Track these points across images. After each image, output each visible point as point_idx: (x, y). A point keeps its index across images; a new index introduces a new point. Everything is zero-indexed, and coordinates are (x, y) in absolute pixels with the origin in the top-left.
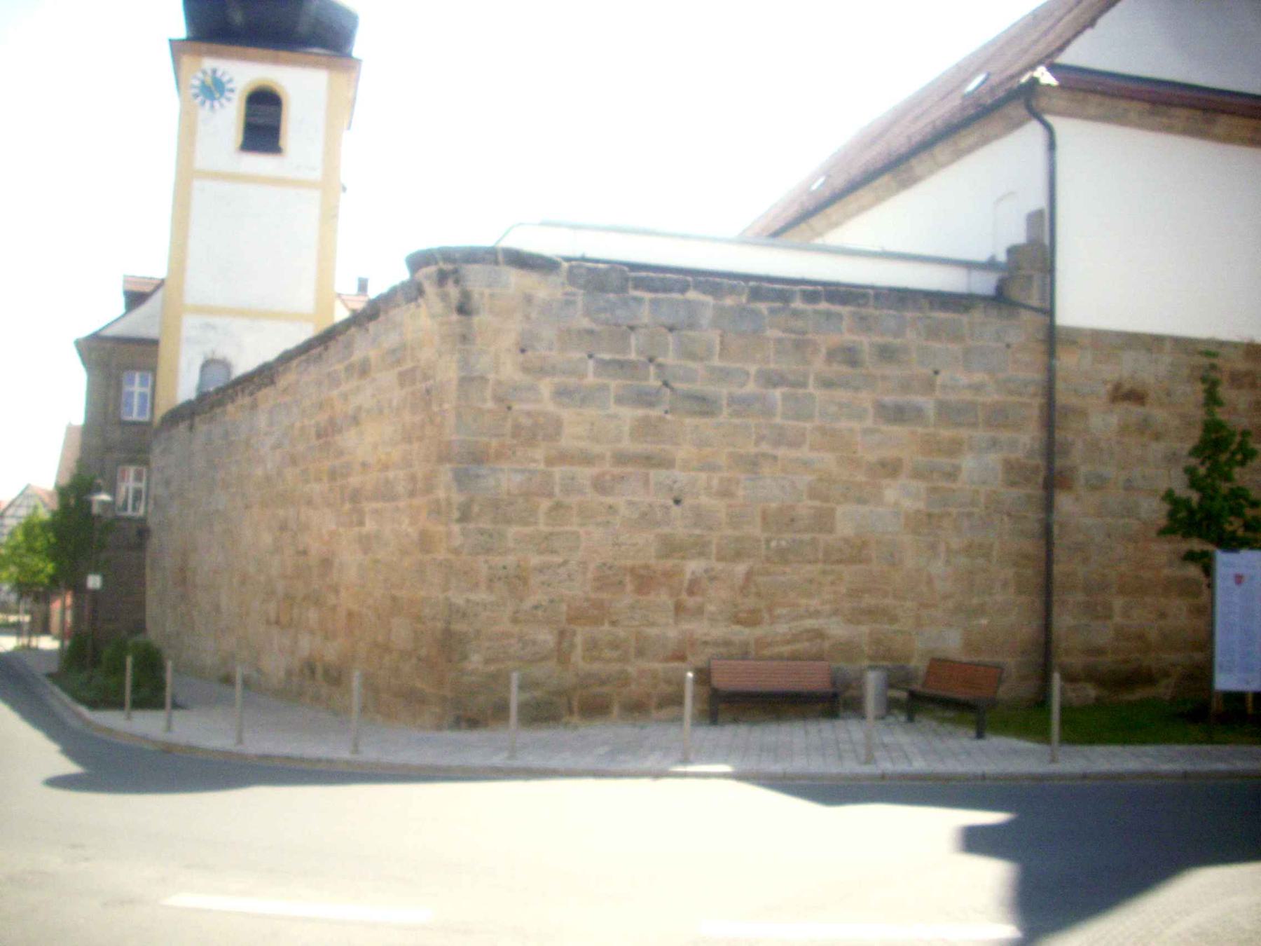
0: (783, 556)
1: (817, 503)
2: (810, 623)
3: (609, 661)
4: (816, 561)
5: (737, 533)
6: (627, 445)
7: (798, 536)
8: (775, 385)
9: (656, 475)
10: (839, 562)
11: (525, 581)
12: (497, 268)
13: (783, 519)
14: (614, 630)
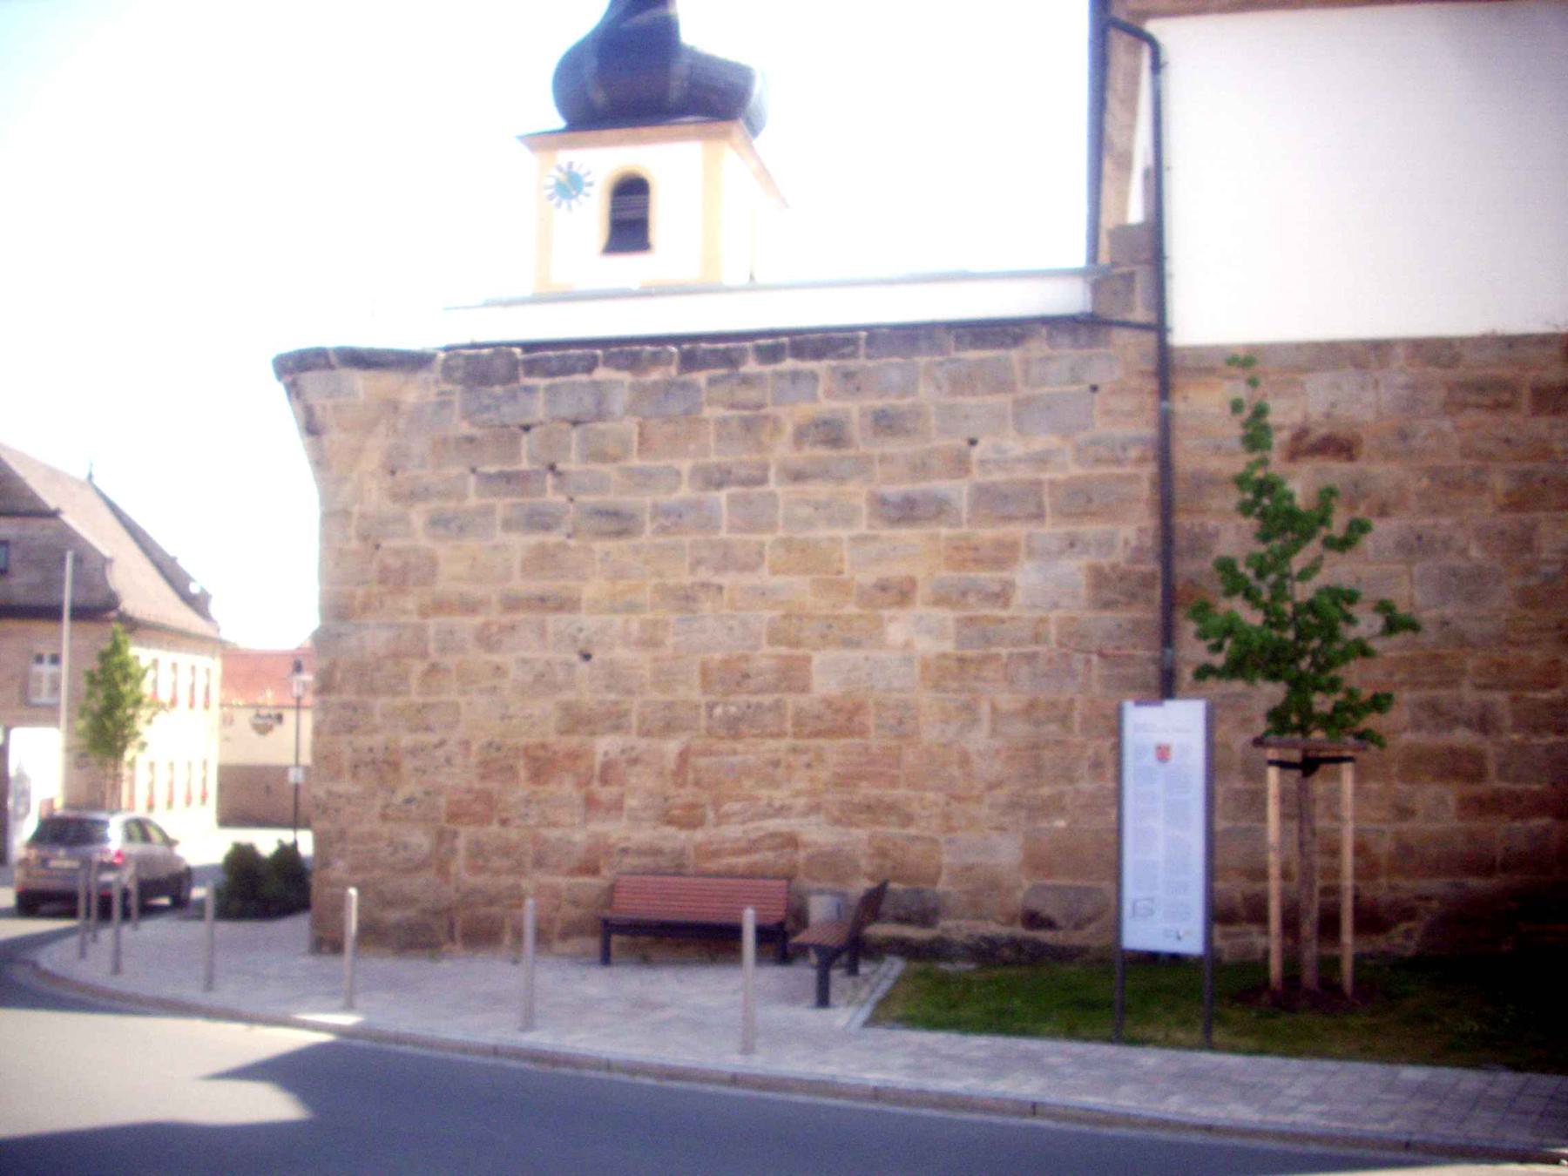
1: (783, 650)
2: (773, 824)
3: (497, 872)
5: (668, 698)
6: (520, 585)
8: (719, 485)
10: (818, 734)
11: (395, 766)
12: (335, 373)
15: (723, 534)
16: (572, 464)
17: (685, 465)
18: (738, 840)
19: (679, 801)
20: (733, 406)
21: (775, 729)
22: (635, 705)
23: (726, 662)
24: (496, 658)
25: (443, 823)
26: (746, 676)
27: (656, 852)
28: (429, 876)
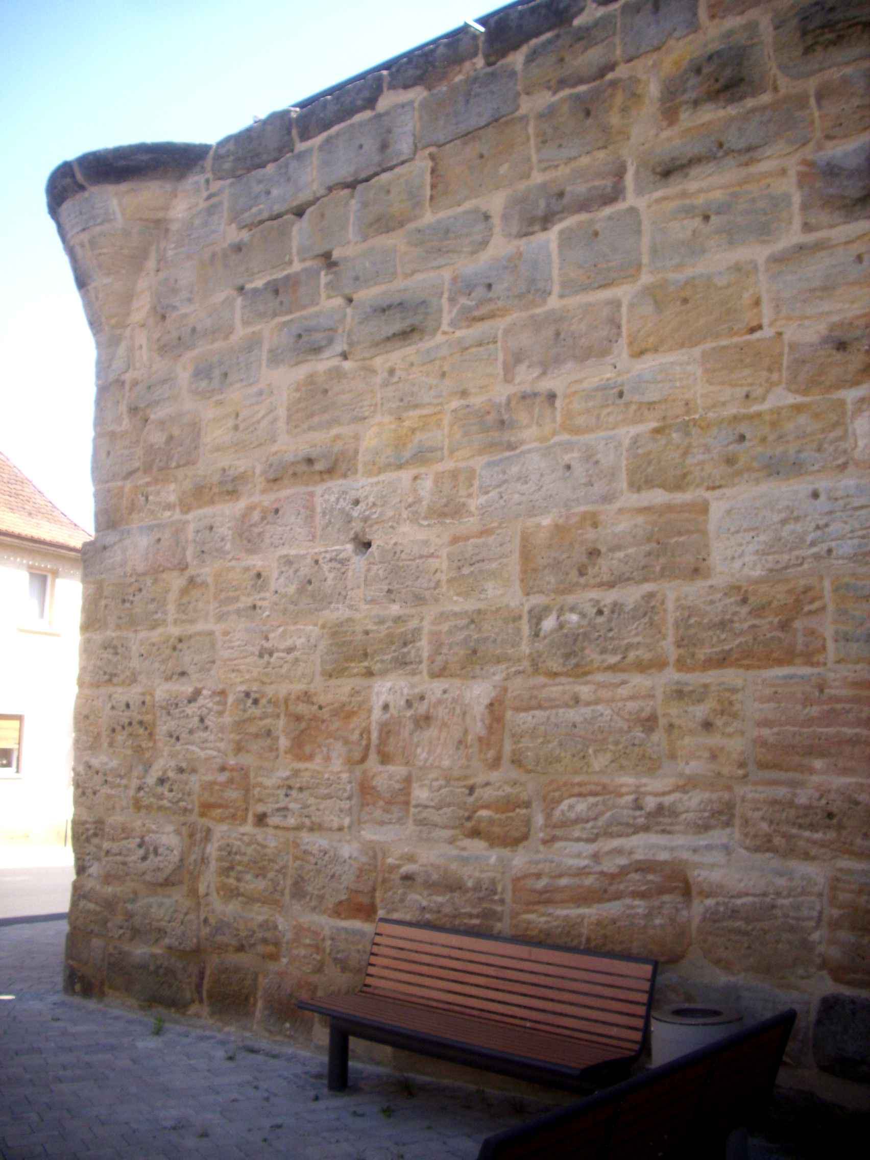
0: (572, 654)
1: (658, 497)
2: (644, 845)
3: (251, 899)
4: (659, 664)
5: (470, 605)
6: (290, 445)
7: (609, 597)
8: (546, 221)
9: (327, 494)
10: (722, 661)
11: (149, 728)
12: (86, 194)
13: (573, 556)
14: (260, 834)
15: (553, 302)
16: (348, 249)
17: (496, 203)
18: (582, 872)
19: (488, 794)
20: (563, 83)
21: (644, 654)
22: (426, 621)
23: (559, 530)
24: (257, 562)
25: (194, 817)
26: (594, 553)
27: (453, 886)
28: (177, 897)
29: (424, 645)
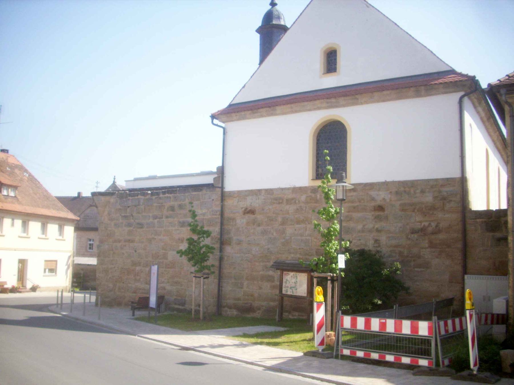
1: (164, 251)
8: (156, 219)
9: (131, 245)
16: (135, 214)
29: (142, 264)
